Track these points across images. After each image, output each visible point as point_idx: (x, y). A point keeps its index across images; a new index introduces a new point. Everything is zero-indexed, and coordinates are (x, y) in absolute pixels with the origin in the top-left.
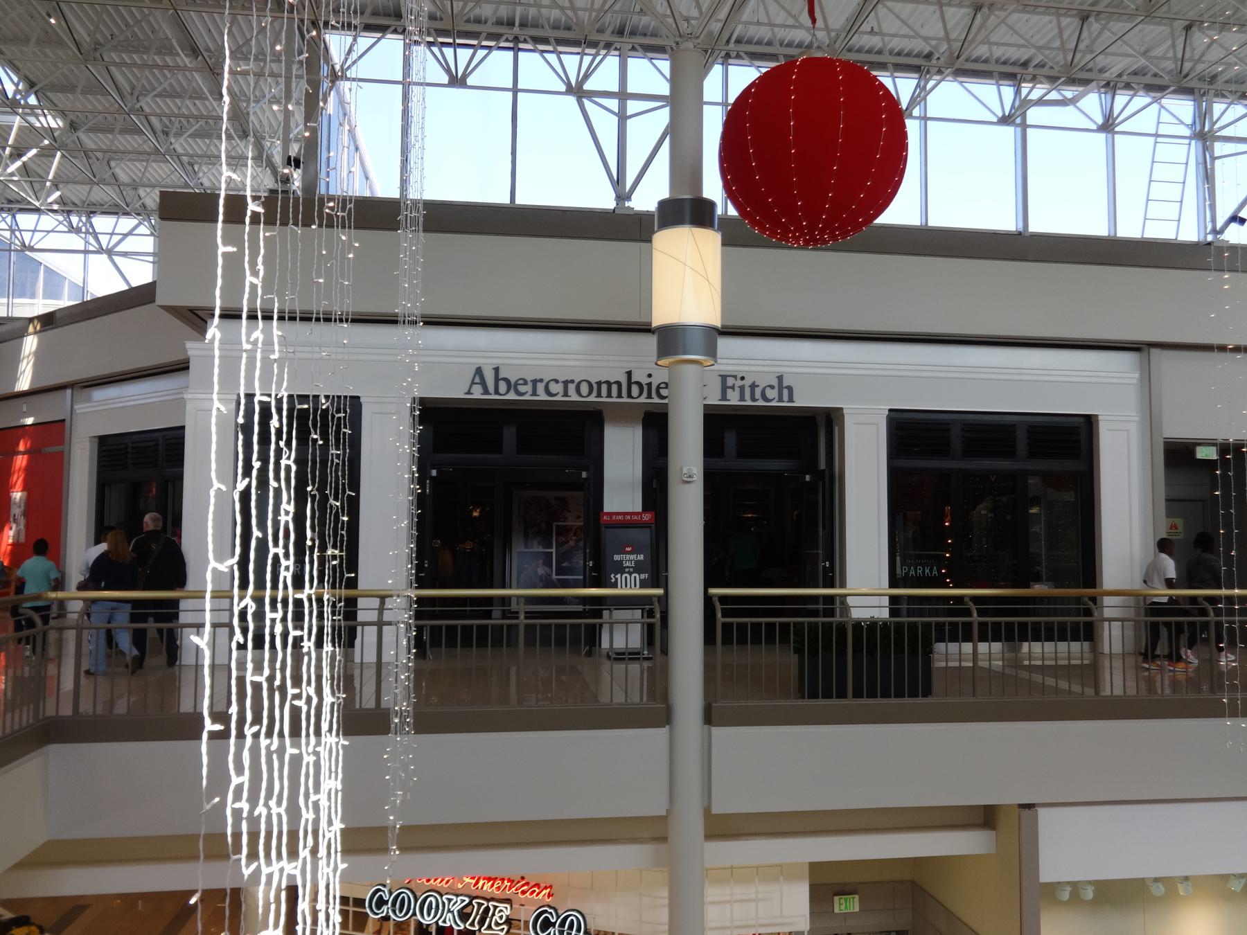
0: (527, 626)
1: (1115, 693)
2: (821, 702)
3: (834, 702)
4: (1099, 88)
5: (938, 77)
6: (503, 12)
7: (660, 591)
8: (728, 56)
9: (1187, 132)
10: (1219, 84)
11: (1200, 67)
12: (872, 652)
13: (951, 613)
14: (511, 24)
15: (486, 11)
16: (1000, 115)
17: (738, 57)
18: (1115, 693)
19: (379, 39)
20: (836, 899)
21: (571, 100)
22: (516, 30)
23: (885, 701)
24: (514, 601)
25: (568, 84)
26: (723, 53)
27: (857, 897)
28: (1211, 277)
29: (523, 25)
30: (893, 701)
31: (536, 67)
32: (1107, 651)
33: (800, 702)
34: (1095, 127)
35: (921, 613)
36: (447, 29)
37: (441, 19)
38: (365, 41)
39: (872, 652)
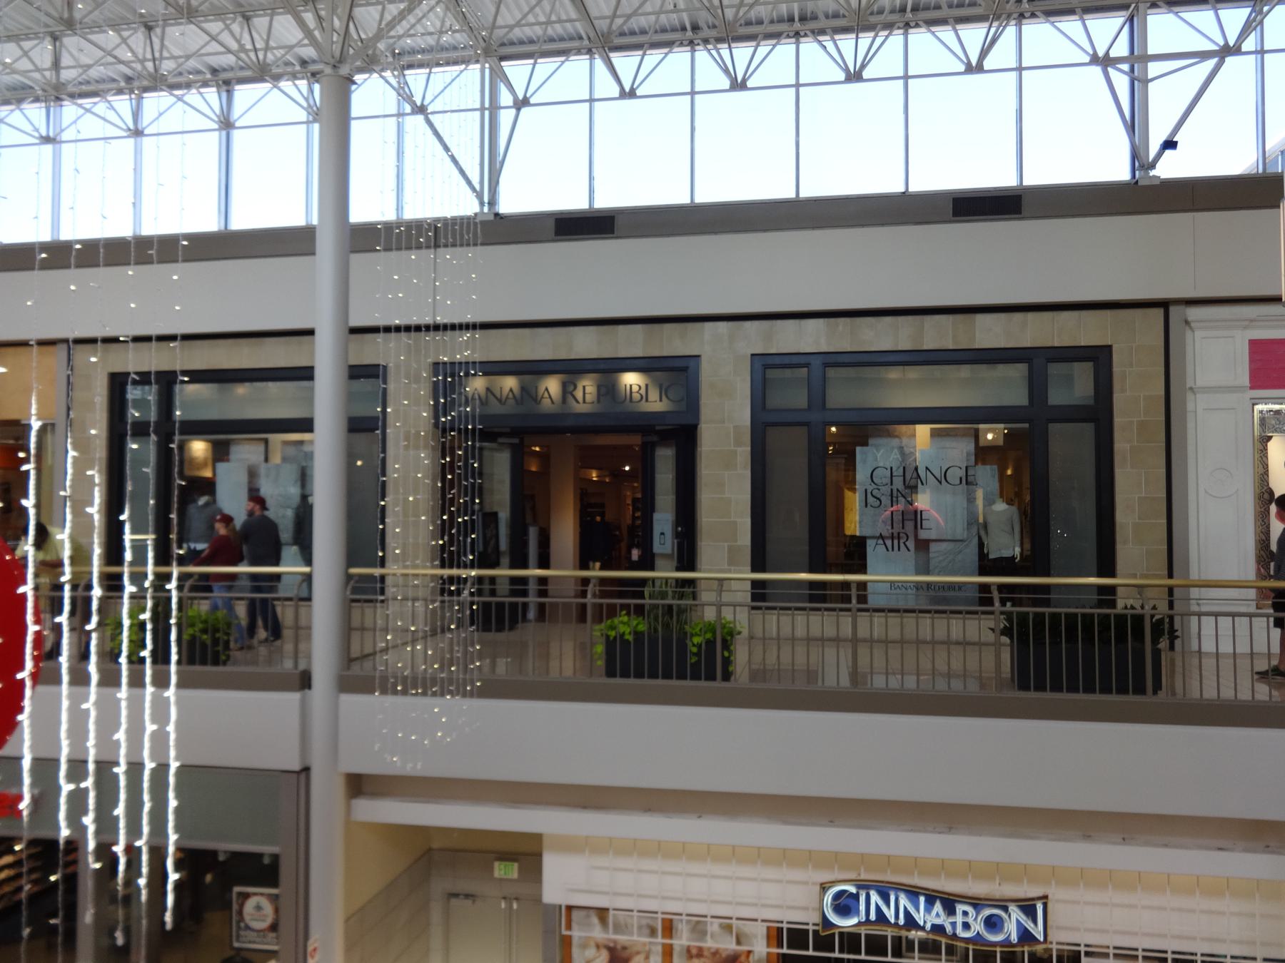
0: (594, 605)
1: (1206, 696)
2: (674, 682)
3: (703, 684)
4: (218, 86)
5: (886, 33)
6: (784, 9)
7: (354, 571)
8: (1022, 16)
9: (216, 126)
10: (706, 33)
11: (619, 21)
12: (1039, 642)
13: (1036, 603)
14: (791, 19)
15: (762, 11)
16: (1222, 43)
17: (1033, 15)
18: (1206, 696)
19: (774, 46)
20: (497, 864)
21: (1097, 70)
22: (797, 25)
23: (1138, 698)
24: (658, 583)
25: (847, 70)
26: (1015, 15)
27: (516, 865)
28: (404, 253)
29: (803, 19)
30: (660, 682)
31: (816, 57)
32: (1195, 647)
33: (1023, 694)
34: (125, 134)
35: (621, 595)
36: (604, 41)
37: (844, 16)
38: (653, 57)
39: (1039, 642)
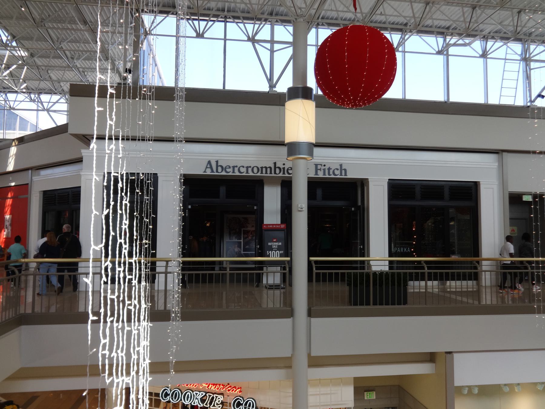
0: (230, 274)
1: (487, 303)
2: (359, 307)
3: (365, 307)
4: (480, 38)
5: (410, 34)
6: (220, 5)
7: (289, 259)
8: (318, 24)
9: (519, 58)
10: (533, 37)
11: (525, 29)
12: (381, 285)
13: (416, 268)
14: (223, 10)
15: (213, 5)
16: (437, 50)
17: (323, 25)
18: (487, 303)
19: (166, 17)
20: (366, 393)
21: (250, 44)
22: (226, 13)
23: (387, 307)
24: (225, 263)
25: (248, 37)
26: (316, 23)
27: (374, 392)
28: (529, 121)
29: (229, 11)
30: (390, 306)
31: (234, 29)
32: (484, 285)
33: (350, 307)
34: (478, 56)
35: (403, 268)
36: (195, 13)
37: (193, 8)
38: (159, 18)
39: (381, 285)
